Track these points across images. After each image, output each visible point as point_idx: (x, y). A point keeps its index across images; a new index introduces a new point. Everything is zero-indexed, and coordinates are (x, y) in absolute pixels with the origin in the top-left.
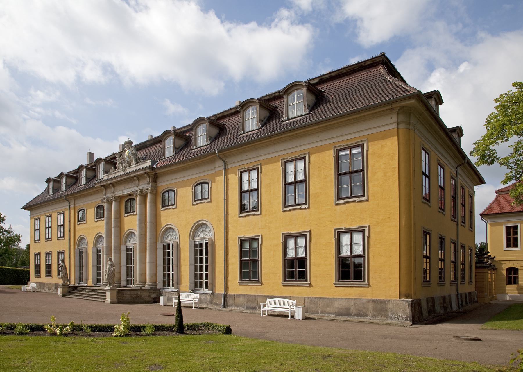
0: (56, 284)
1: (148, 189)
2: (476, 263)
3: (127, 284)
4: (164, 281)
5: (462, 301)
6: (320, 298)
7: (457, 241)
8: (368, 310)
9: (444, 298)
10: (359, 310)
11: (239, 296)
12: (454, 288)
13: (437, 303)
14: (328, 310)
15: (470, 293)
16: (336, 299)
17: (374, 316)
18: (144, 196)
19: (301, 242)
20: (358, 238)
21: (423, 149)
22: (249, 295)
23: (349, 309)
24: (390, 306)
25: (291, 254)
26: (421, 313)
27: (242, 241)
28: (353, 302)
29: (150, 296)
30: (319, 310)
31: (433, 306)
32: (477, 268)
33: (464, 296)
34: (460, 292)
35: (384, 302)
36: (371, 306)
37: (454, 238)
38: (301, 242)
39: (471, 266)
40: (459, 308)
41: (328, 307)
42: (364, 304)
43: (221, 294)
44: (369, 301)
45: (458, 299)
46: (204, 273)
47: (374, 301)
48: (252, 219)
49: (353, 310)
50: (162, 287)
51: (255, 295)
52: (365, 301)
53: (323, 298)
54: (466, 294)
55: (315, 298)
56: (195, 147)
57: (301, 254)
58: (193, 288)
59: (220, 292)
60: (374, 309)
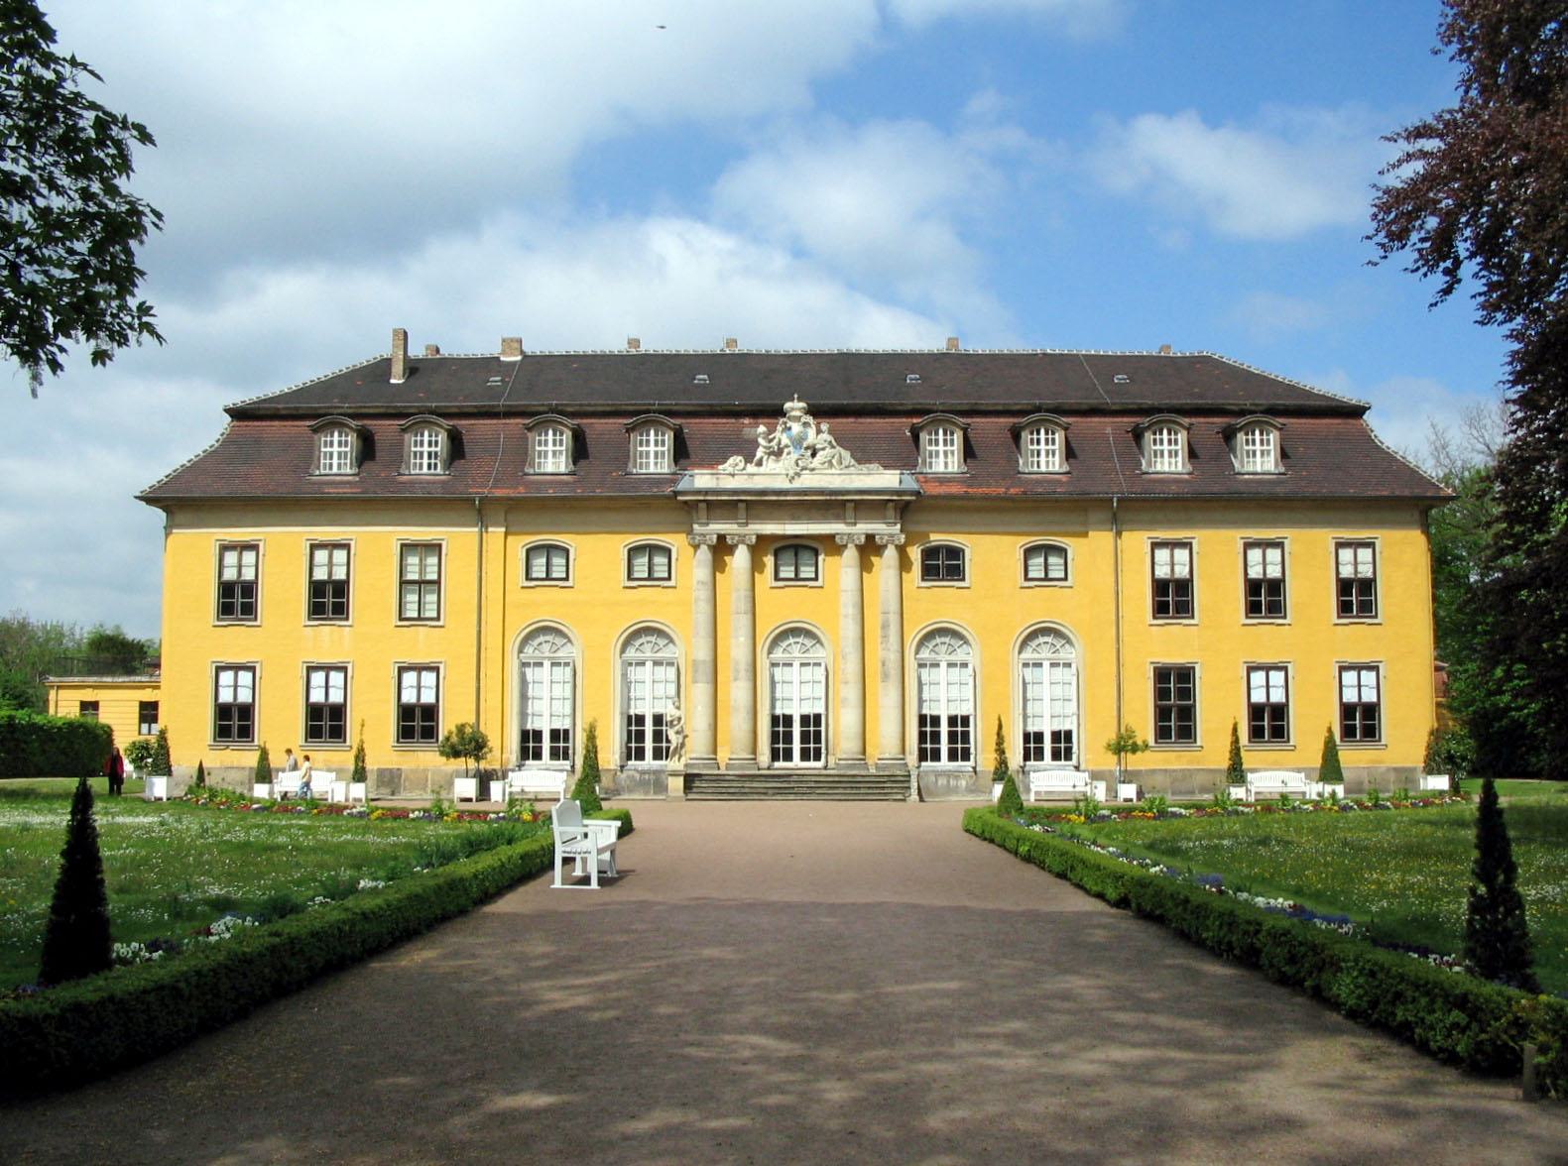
11: (1154, 771)
23: (1361, 783)
27: (1162, 674)
36: (1392, 777)
44: (1389, 769)
51: (1189, 770)
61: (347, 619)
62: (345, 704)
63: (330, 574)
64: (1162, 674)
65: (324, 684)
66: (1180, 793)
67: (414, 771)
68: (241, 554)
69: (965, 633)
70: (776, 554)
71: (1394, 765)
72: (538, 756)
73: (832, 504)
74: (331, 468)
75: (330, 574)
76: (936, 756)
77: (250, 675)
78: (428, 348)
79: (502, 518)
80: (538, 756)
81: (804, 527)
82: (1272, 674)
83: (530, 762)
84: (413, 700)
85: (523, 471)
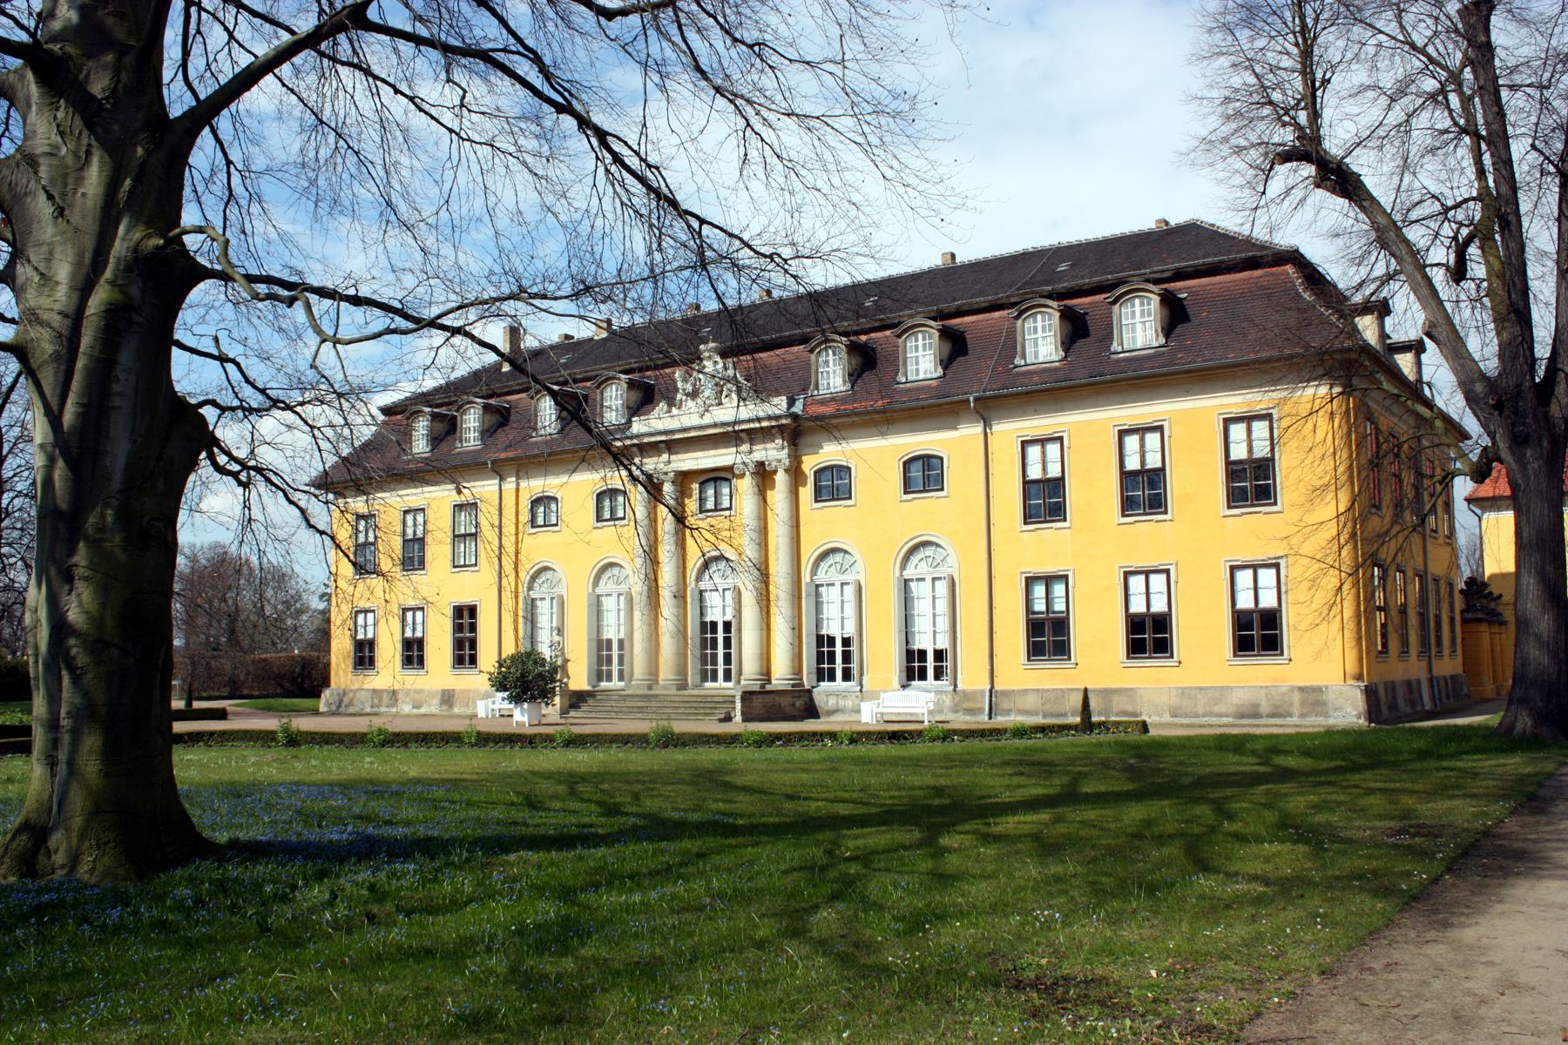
0: (444, 691)
1: (780, 461)
2: (1462, 612)
3: (704, 679)
4: (818, 669)
5: (1439, 690)
6: (1201, 689)
7: (1426, 571)
8: (1291, 704)
9: (1408, 684)
10: (1277, 707)
11: (1025, 691)
12: (1424, 664)
13: (1400, 692)
14: (1216, 709)
15: (1453, 677)
16: (1232, 688)
17: (1302, 715)
18: (763, 475)
19: (1158, 581)
20: (1267, 577)
21: (1369, 420)
22: (1048, 690)
23: (1257, 706)
24: (1330, 697)
25: (1138, 606)
26: (1379, 711)
27: (459, 611)
28: (1263, 691)
29: (794, 704)
30: (1200, 710)
31: (1395, 697)
32: (1464, 621)
33: (1442, 683)
34: (1436, 672)
35: (1317, 690)
36: (1296, 697)
37: (1420, 567)
38: (1158, 581)
39: (1452, 620)
40: (1436, 705)
41: (1216, 704)
42: (1284, 694)
43: (983, 692)
44: (1292, 689)
45: (1432, 687)
46: (721, 651)
47: (1301, 689)
48: (1049, 533)
49: (1265, 707)
50: (814, 683)
51: (1062, 690)
52: (1284, 689)
53: (1207, 688)
54: (1445, 678)
55: (1191, 688)
56: (904, 380)
57: (1159, 606)
58: (905, 682)
59: (978, 687)
60: (1303, 703)
61: (1275, 503)
62: (1169, 614)
63: (1143, 462)
64: (459, 611)
65: (1252, 585)
66: (1052, 715)
67: (463, 691)
68: (1043, 446)
69: (546, 564)
70: (702, 484)
71: (1300, 685)
72: (923, 676)
73: (731, 436)
74: (917, 374)
75: (1143, 462)
76: (832, 678)
77: (1273, 572)
78: (1158, 221)
79: (514, 472)
80: (923, 676)
81: (1239, 399)
82: (1261, 572)
83: (916, 683)
84: (1143, 609)
85: (895, 379)
